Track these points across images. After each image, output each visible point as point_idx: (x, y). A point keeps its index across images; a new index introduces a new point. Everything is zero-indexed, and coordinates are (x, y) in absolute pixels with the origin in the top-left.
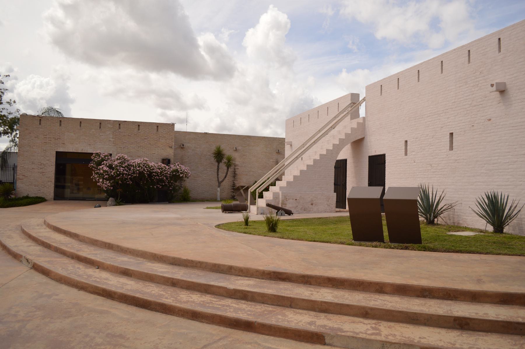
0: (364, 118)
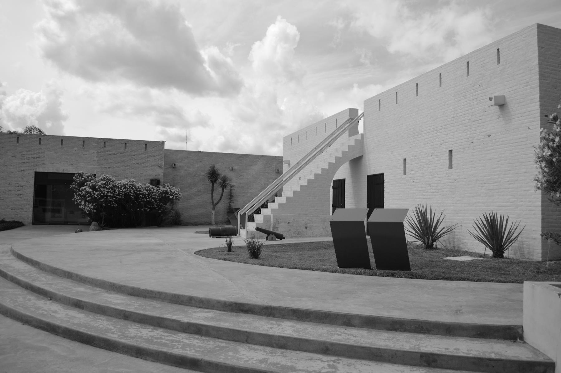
0: (362, 135)
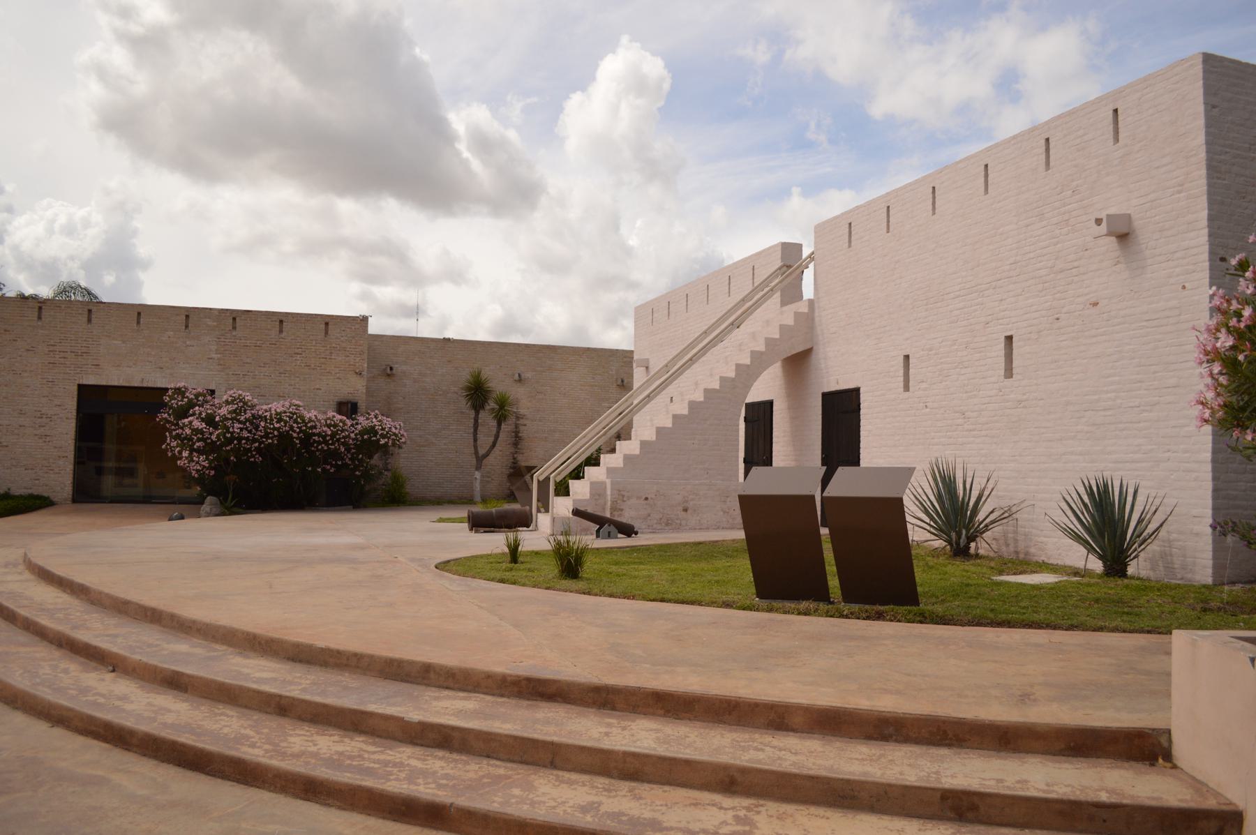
0: (811, 302)
